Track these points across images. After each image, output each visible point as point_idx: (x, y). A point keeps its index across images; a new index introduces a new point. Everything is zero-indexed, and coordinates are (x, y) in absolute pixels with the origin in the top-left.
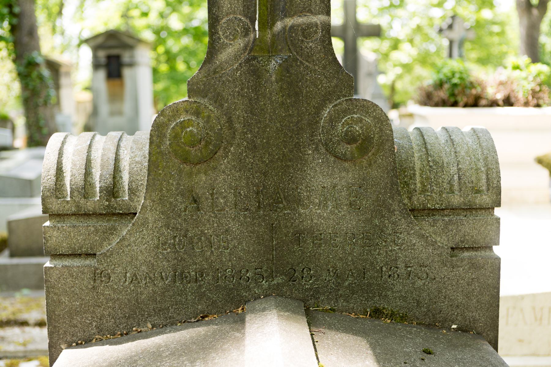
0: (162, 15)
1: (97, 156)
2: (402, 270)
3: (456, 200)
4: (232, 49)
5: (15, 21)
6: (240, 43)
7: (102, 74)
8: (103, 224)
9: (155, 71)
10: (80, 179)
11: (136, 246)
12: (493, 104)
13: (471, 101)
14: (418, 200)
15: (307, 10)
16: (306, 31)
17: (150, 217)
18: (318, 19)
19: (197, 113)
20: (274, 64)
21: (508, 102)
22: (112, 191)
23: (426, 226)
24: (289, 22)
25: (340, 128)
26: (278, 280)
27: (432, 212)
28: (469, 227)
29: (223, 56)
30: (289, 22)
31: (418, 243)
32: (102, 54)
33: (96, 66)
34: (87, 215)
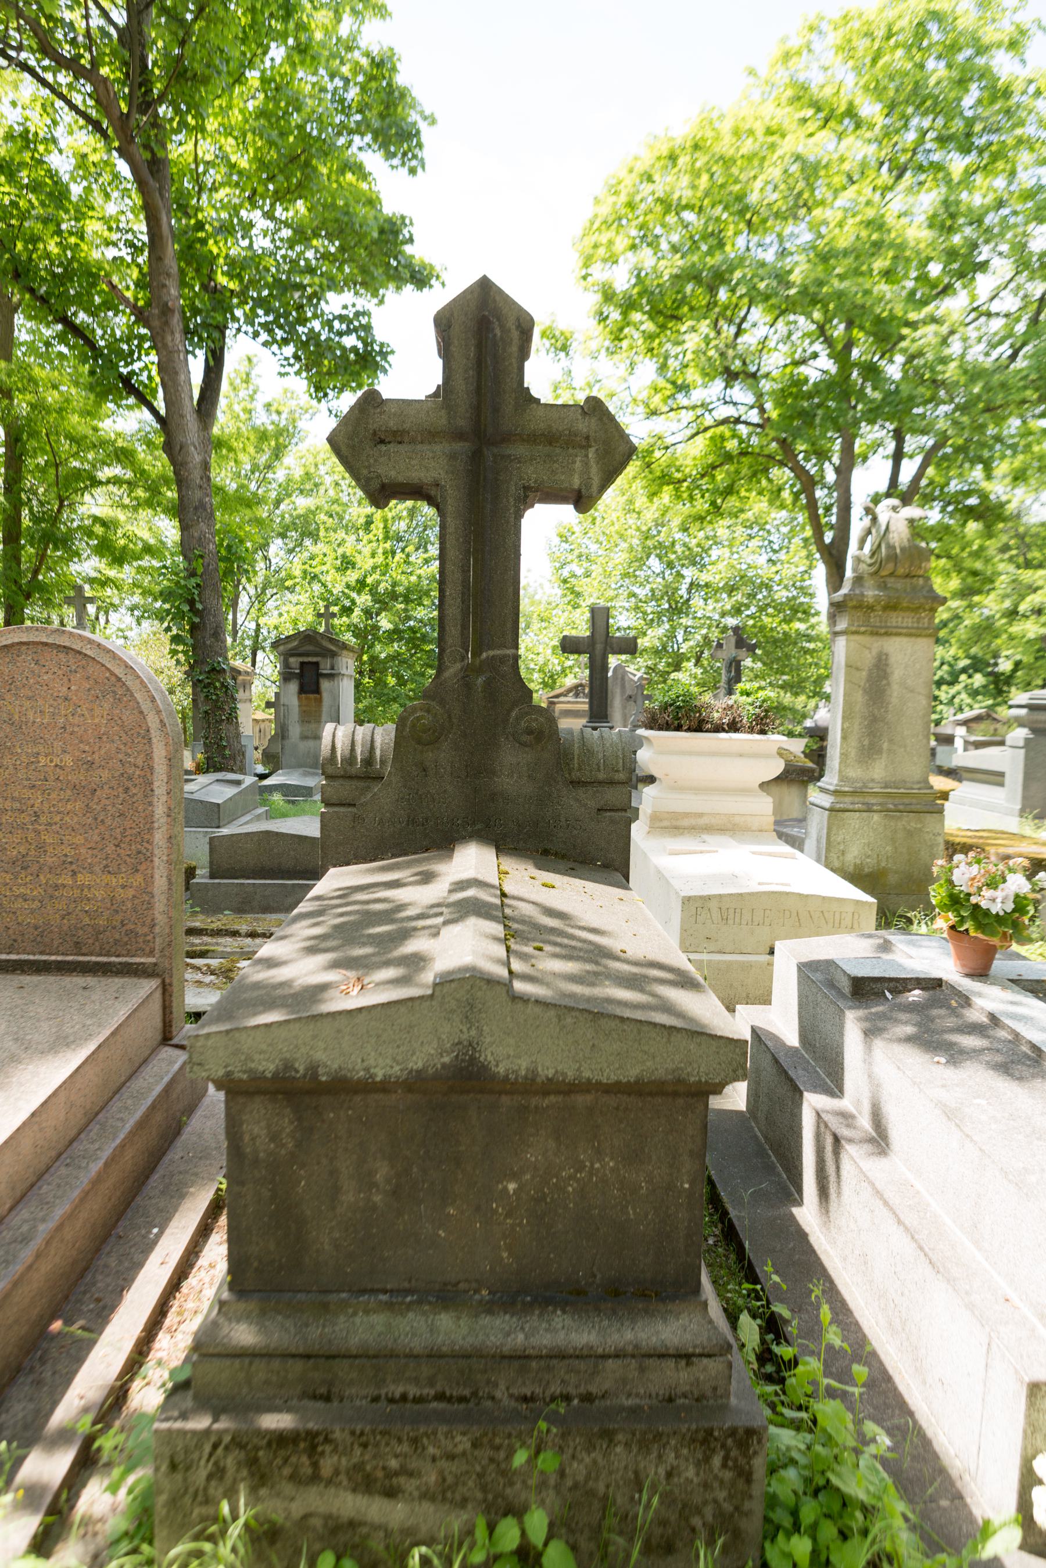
0: (367, 613)
1: (359, 738)
2: (563, 823)
3: (601, 776)
4: (453, 669)
5: (197, 620)
6: (458, 666)
7: (293, 687)
8: (361, 784)
9: (358, 685)
10: (347, 752)
11: (383, 799)
12: (718, 729)
13: (694, 724)
14: (576, 775)
15: (503, 646)
16: (503, 659)
17: (394, 780)
18: (510, 652)
19: (428, 711)
20: (480, 680)
21: (734, 727)
22: (369, 761)
23: (581, 793)
24: (491, 653)
25: (523, 724)
26: (479, 826)
27: (585, 784)
28: (611, 796)
29: (447, 674)
30: (491, 653)
31: (575, 805)
32: (294, 661)
33: (286, 676)
34: (351, 777)
